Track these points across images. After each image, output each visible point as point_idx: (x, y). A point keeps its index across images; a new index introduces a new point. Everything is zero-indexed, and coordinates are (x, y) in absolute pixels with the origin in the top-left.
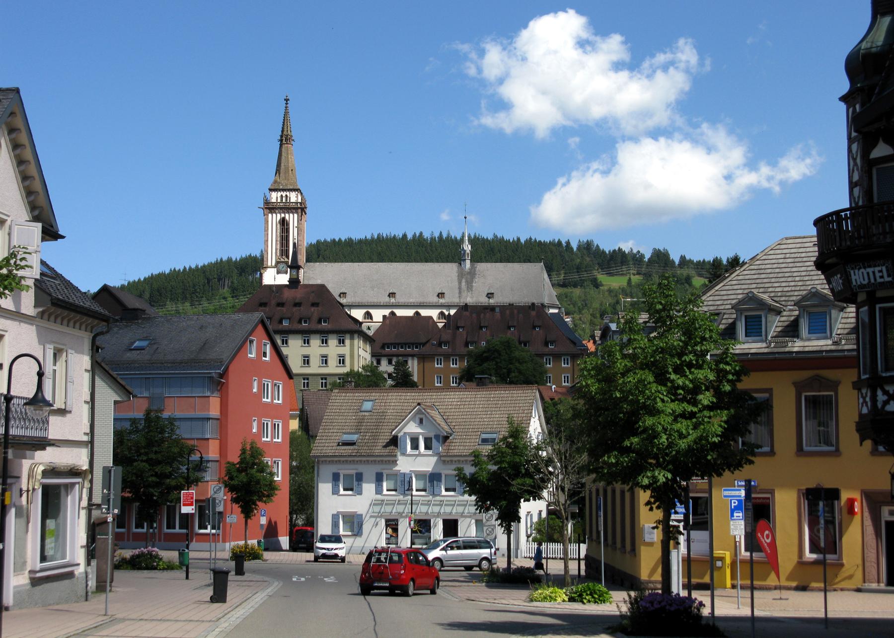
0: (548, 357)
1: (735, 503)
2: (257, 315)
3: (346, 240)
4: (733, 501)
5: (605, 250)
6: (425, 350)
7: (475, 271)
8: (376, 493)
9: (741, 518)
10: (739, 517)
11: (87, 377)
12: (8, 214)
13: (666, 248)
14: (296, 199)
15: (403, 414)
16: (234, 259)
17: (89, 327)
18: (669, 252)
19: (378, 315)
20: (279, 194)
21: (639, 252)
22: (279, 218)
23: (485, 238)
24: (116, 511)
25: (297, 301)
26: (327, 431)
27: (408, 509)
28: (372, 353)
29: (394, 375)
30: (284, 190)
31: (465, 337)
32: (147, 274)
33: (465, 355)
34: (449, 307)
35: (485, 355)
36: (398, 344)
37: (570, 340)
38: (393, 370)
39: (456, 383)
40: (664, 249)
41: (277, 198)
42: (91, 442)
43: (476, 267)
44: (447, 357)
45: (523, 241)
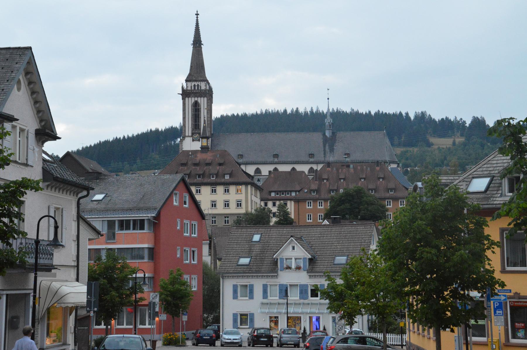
0: (389, 200)
1: (497, 304)
2: (179, 177)
3: (242, 114)
4: (495, 303)
5: (435, 119)
6: (300, 195)
7: (335, 137)
8: (263, 298)
9: (502, 314)
10: (500, 313)
11: (74, 225)
12: (26, 125)
13: (482, 116)
14: (205, 87)
15: (281, 243)
16: (160, 130)
17: (75, 194)
18: (485, 119)
19: (265, 170)
20: (193, 84)
21: (461, 119)
22: (193, 101)
23: (345, 111)
24: (96, 309)
25: (207, 162)
26: (228, 255)
27: (284, 311)
28: (261, 198)
29: (277, 214)
30: (196, 81)
31: (328, 186)
32: (96, 141)
33: (329, 199)
34: (317, 163)
35: (343, 198)
36: (280, 191)
37: (404, 186)
38: (276, 211)
39: (322, 220)
40: (481, 117)
41: (191, 86)
42: (78, 266)
43: (336, 135)
44: (315, 200)
45: (373, 113)
